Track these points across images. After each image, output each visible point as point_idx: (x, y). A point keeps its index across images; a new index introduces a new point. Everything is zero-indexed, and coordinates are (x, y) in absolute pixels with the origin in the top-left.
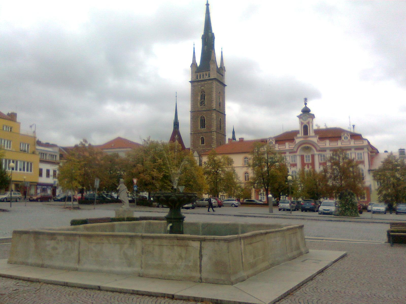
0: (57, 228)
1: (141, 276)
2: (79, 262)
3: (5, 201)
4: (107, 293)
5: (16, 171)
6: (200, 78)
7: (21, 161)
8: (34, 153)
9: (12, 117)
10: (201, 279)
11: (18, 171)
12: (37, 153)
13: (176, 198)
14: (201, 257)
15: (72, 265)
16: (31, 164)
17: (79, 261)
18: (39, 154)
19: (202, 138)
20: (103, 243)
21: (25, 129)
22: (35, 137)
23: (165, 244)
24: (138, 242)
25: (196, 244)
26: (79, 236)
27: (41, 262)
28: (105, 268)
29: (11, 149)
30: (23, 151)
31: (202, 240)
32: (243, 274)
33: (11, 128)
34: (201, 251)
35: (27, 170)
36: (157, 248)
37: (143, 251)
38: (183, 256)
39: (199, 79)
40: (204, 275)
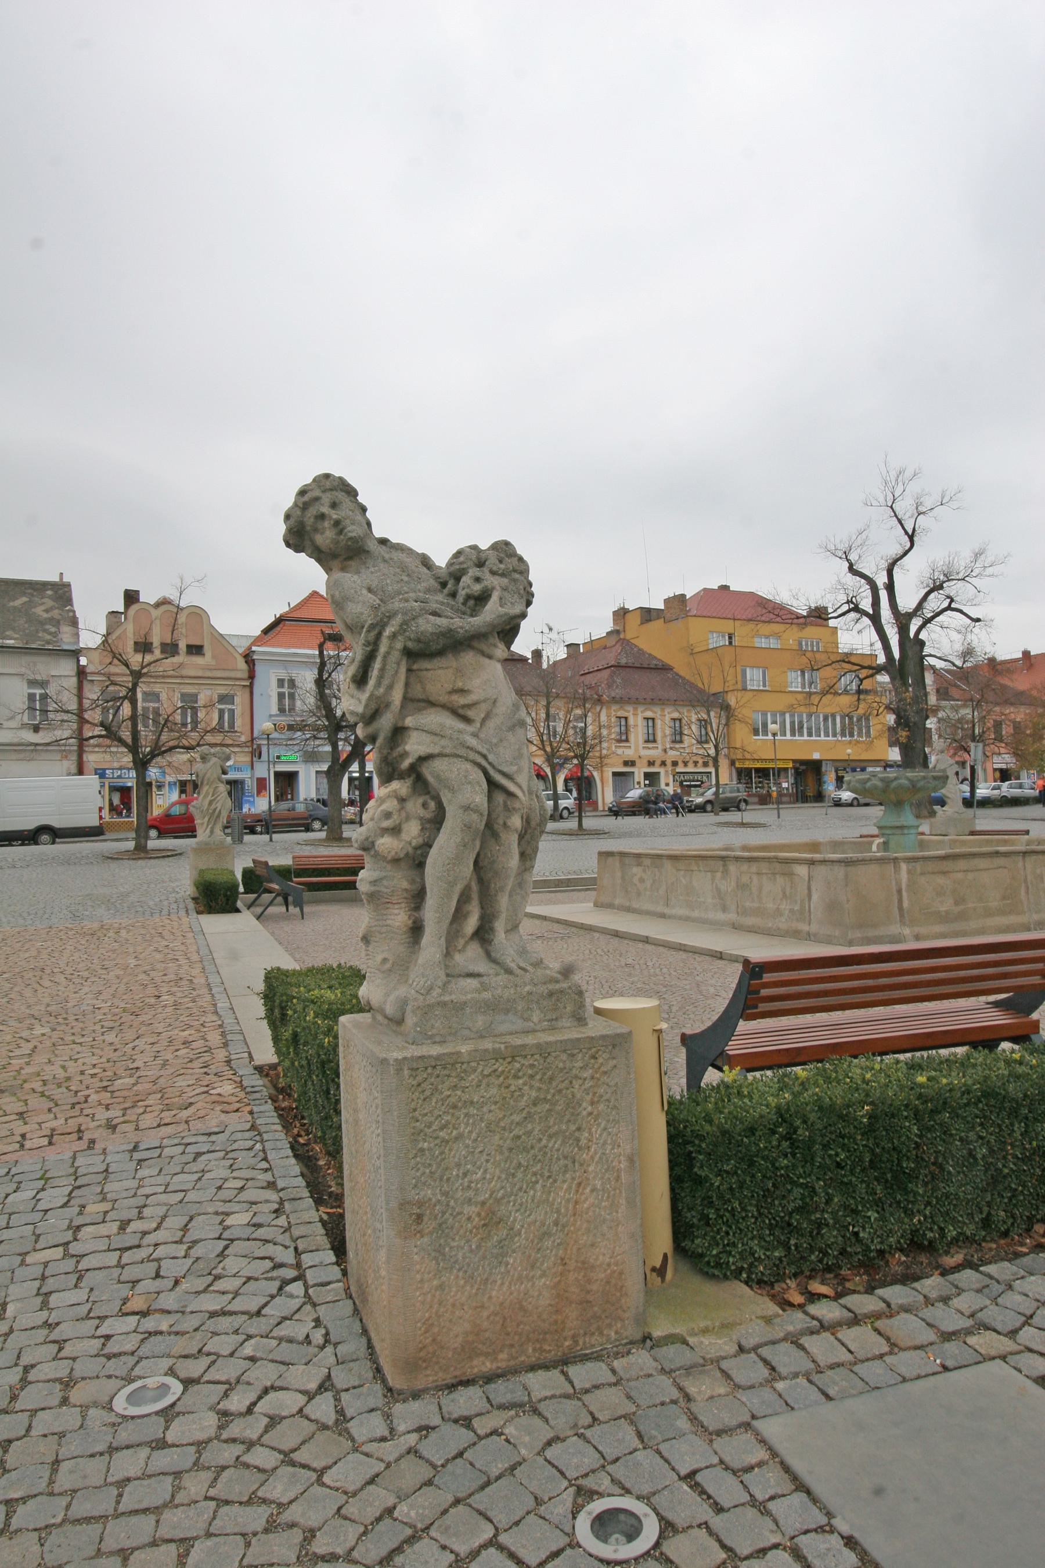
1: (736, 927)
3: (855, 803)
13: (906, 782)
15: (660, 909)
25: (802, 870)
27: (627, 904)
36: (755, 878)
37: (742, 887)
38: (788, 893)
40: (814, 928)
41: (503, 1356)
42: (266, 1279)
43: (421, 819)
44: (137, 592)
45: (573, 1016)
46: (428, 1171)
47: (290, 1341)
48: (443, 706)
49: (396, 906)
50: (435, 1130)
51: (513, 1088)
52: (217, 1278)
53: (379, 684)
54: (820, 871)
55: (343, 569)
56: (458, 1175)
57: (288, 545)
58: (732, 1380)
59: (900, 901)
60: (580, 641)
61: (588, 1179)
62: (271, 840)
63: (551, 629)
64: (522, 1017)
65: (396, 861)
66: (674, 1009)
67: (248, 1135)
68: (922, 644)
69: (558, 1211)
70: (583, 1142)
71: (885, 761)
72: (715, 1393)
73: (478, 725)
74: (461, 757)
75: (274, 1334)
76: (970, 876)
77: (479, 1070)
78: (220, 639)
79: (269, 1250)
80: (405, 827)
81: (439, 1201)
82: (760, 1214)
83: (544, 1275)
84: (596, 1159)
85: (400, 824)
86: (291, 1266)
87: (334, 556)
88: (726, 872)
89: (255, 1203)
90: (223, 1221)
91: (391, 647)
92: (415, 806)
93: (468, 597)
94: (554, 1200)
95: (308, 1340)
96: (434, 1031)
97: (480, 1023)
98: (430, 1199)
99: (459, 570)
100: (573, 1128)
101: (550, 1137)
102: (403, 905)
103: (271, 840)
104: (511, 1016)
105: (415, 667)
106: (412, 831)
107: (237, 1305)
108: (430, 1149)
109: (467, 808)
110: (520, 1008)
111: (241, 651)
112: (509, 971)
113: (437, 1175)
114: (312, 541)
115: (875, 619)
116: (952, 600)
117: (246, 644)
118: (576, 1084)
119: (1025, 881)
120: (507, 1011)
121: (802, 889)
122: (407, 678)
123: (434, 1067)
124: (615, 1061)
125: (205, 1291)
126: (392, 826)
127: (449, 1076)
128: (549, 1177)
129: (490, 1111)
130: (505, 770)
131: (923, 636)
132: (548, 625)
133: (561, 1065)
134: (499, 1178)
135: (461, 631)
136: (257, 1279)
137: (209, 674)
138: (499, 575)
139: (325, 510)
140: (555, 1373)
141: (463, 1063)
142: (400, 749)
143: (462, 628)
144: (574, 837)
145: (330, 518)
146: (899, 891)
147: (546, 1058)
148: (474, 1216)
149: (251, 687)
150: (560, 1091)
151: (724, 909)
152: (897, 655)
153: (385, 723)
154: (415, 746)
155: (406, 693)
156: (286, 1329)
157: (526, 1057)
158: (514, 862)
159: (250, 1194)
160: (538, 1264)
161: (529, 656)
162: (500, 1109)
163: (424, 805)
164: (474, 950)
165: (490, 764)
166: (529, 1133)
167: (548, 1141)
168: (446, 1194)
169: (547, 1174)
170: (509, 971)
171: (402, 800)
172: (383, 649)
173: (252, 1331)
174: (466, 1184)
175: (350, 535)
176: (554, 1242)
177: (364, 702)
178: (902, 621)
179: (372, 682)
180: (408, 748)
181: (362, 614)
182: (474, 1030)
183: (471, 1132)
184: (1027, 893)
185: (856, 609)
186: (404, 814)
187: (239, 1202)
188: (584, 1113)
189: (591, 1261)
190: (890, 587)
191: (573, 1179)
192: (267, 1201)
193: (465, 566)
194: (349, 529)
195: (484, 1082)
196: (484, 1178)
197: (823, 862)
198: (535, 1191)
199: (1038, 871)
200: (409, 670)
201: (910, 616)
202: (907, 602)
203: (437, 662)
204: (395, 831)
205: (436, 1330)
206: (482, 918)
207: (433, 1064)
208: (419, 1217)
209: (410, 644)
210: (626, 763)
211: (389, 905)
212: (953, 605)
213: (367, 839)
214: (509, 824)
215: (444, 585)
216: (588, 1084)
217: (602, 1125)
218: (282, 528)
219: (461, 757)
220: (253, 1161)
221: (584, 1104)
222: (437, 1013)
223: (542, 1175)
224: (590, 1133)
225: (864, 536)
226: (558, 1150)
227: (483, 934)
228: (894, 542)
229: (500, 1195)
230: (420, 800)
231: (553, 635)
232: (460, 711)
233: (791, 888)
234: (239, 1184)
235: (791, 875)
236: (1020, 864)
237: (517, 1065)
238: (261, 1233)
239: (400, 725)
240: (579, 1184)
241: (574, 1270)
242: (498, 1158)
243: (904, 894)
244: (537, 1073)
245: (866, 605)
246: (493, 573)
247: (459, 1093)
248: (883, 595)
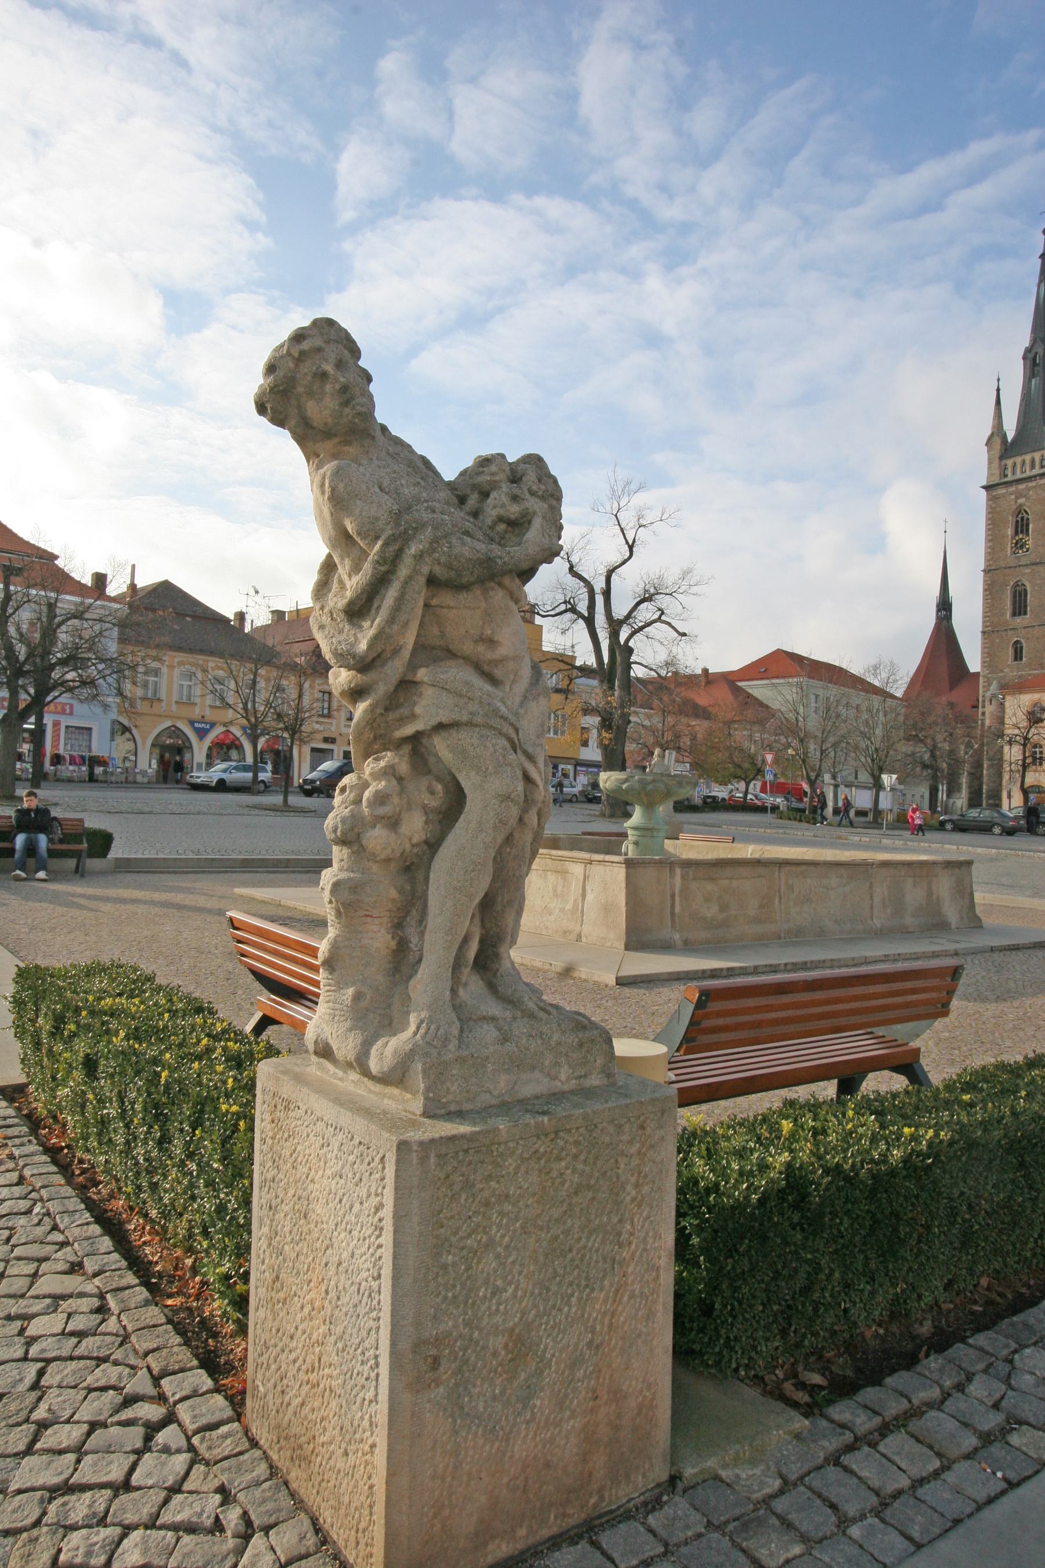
3: (574, 799)
6: (1014, 473)
19: (1017, 642)
39: (1009, 478)
41: (522, 1532)
42: (120, 1423)
45: (603, 1072)
46: (450, 1294)
47: (191, 1529)
48: (467, 659)
49: (376, 921)
50: (462, 1238)
51: (554, 1174)
52: (43, 1425)
53: (391, 620)
56: (485, 1296)
57: (261, 409)
58: (796, 1529)
60: (286, 609)
61: (626, 1283)
63: (257, 592)
64: (549, 1075)
67: (17, 1191)
68: (630, 651)
69: (593, 1332)
70: (625, 1236)
71: (576, 760)
72: (790, 1555)
74: (494, 729)
75: (166, 1518)
76: (735, 883)
77: (518, 1152)
79: (108, 1373)
81: (461, 1336)
82: (769, 1300)
83: (573, 1416)
84: (636, 1259)
86: (151, 1399)
87: (327, 434)
89: (64, 1297)
90: (21, 1332)
91: (416, 571)
94: (590, 1315)
95: (218, 1526)
96: (450, 1097)
97: (502, 1085)
98: (451, 1334)
99: (490, 483)
100: (615, 1220)
101: (590, 1233)
104: (537, 1074)
105: (434, 602)
106: (415, 826)
107: (86, 1473)
108: (454, 1264)
110: (547, 1063)
112: (531, 1016)
113: (461, 1298)
114: (300, 408)
115: (590, 622)
116: (663, 613)
118: (623, 1161)
119: (779, 891)
120: (533, 1068)
121: (575, 887)
122: (423, 616)
123: (466, 1151)
124: (662, 1132)
125: (29, 1451)
127: (482, 1162)
128: (587, 1286)
129: (527, 1206)
131: (631, 644)
132: (254, 587)
133: (607, 1139)
134: (532, 1294)
135: (499, 562)
136: (104, 1425)
138: (538, 497)
139: (329, 368)
140: (583, 1545)
141: (499, 1144)
143: (500, 558)
144: (279, 813)
145: (336, 380)
146: (673, 896)
147: (591, 1131)
150: (604, 1174)
152: (606, 660)
156: (179, 1511)
157: (569, 1131)
159: (47, 1284)
160: (568, 1402)
161: (232, 617)
162: (538, 1202)
166: (567, 1232)
167: (588, 1238)
168: (467, 1324)
169: (583, 1283)
172: (403, 572)
173: (130, 1518)
174: (494, 1308)
175: (359, 408)
176: (585, 1371)
178: (614, 626)
181: (377, 519)
182: (496, 1093)
183: (503, 1236)
184: (780, 902)
185: (573, 610)
187: (37, 1297)
188: (628, 1198)
189: (624, 1388)
190: (607, 593)
191: (611, 1285)
192: (82, 1295)
193: (497, 478)
194: (357, 400)
195: (523, 1169)
196: (515, 1297)
198: (570, 1306)
199: (790, 882)
201: (621, 623)
202: (620, 611)
203: (464, 597)
204: (393, 823)
205: (446, 1512)
207: (466, 1147)
208: (436, 1362)
209: (438, 570)
210: (326, 740)
211: (369, 919)
212: (663, 618)
214: (526, 820)
215: (462, 500)
216: (635, 1162)
217: (645, 1214)
219: (494, 729)
220: (39, 1231)
221: (629, 1188)
222: (454, 1072)
223: (578, 1285)
224: (632, 1225)
225: (585, 540)
226: (597, 1251)
228: (612, 550)
229: (531, 1316)
231: (258, 598)
233: (564, 887)
234: (30, 1268)
235: (564, 873)
237: (561, 1143)
238: (89, 1345)
239: (409, 677)
240: (617, 1291)
241: (606, 1404)
242: (532, 1268)
243: (677, 899)
244: (581, 1152)
245: (583, 607)
246: (533, 494)
248: (600, 600)
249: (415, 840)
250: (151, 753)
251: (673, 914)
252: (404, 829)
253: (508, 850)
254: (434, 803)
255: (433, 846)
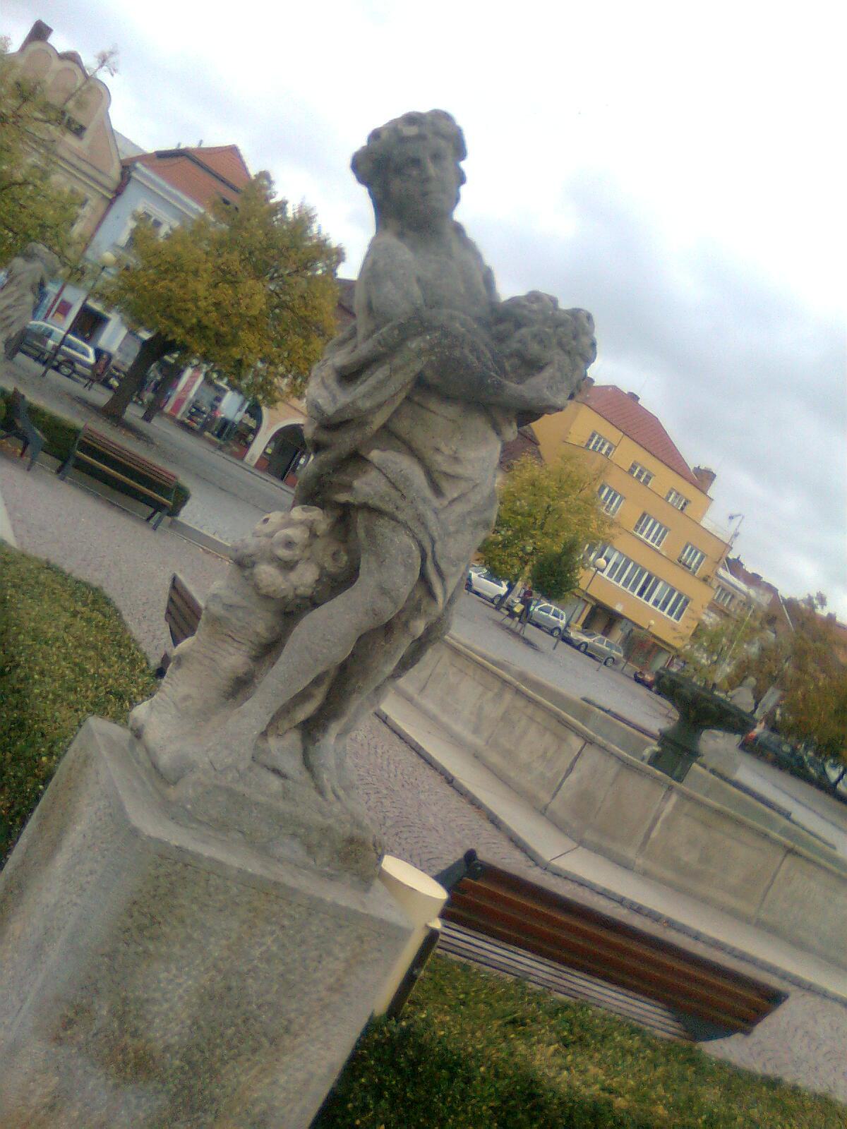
0: (467, 642)
1: (477, 756)
2: (421, 691)
3: (583, 648)
4: (751, 1040)
5: (645, 602)
7: (666, 584)
8: (705, 580)
9: (703, 479)
10: (546, 808)
11: (650, 603)
12: (715, 585)
14: (570, 770)
16: (686, 602)
17: (422, 689)
18: (719, 587)
20: (466, 674)
21: (714, 519)
22: (729, 547)
23: (539, 720)
24: (508, 696)
25: (576, 743)
26: (516, 693)
28: (445, 719)
29: (658, 548)
30: (684, 564)
31: (589, 741)
32: (631, 853)
33: (685, 504)
34: (575, 760)
35: (671, 613)
37: (505, 718)
38: (549, 755)
40: (555, 805)
43: (322, 568)
44: (49, 31)
49: (235, 645)
53: (367, 395)
54: (592, 756)
55: (400, 235)
59: (651, 829)
62: (44, 374)
65: (267, 597)
66: (389, 823)
73: (446, 503)
78: (108, 133)
80: (301, 567)
85: (297, 562)
88: (499, 696)
92: (324, 550)
93: (518, 354)
102: (244, 648)
103: (44, 374)
106: (305, 577)
109: (384, 591)
111: (123, 157)
112: (321, 792)
117: (133, 154)
121: (565, 762)
126: (288, 559)
130: (443, 566)
137: (74, 161)
142: (346, 479)
146: (656, 819)
148: (130, 1050)
149: (111, 203)
151: (476, 731)
153: (345, 441)
154: (367, 486)
155: (389, 420)
158: (389, 669)
163: (335, 556)
164: (294, 738)
165: (433, 552)
170: (321, 792)
171: (313, 535)
177: (339, 405)
179: (361, 389)
180: (356, 483)
186: (307, 554)
197: (603, 748)
200: (408, 399)
204: (287, 566)
206: (321, 709)
209: (429, 373)
211: (229, 640)
213: (251, 556)
218: (361, 142)
227: (312, 729)
230: (333, 548)
232: (436, 475)
236: (780, 858)
239: (363, 453)
243: (659, 825)
247: (195, 907)
249: (299, 591)
250: (269, 442)
251: (647, 836)
252: (293, 577)
253: (383, 643)
254: (330, 566)
255: (313, 602)
